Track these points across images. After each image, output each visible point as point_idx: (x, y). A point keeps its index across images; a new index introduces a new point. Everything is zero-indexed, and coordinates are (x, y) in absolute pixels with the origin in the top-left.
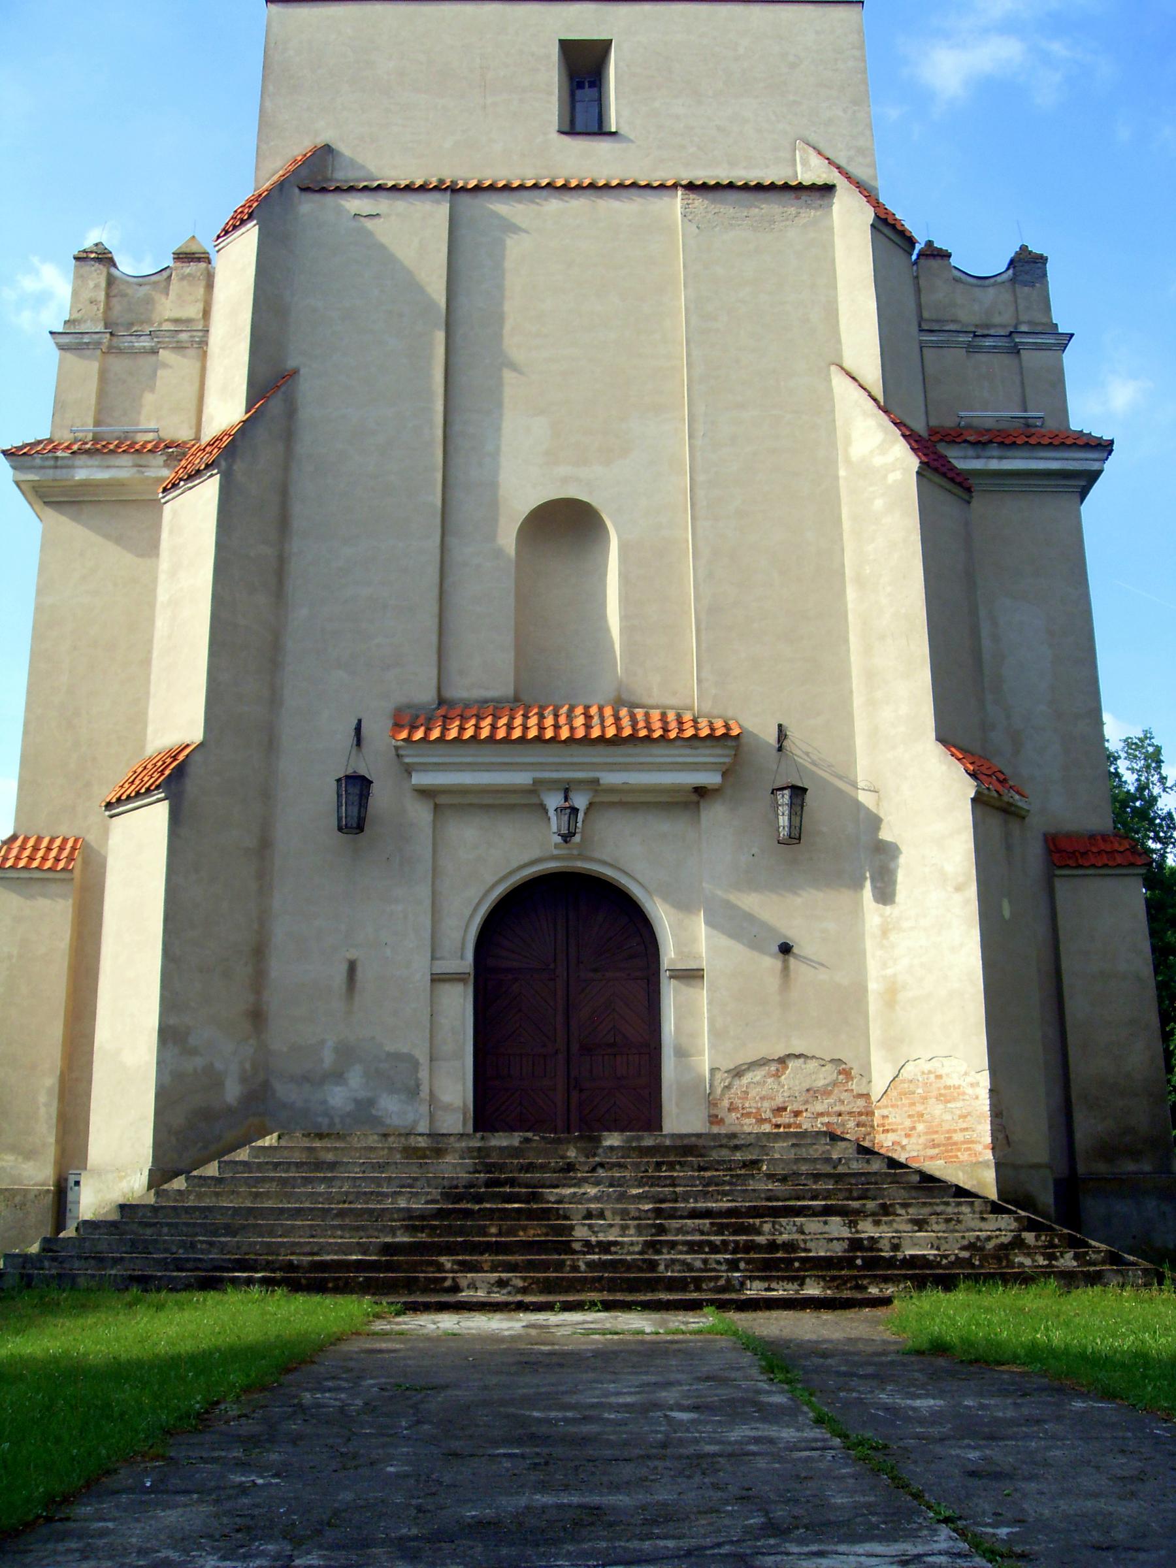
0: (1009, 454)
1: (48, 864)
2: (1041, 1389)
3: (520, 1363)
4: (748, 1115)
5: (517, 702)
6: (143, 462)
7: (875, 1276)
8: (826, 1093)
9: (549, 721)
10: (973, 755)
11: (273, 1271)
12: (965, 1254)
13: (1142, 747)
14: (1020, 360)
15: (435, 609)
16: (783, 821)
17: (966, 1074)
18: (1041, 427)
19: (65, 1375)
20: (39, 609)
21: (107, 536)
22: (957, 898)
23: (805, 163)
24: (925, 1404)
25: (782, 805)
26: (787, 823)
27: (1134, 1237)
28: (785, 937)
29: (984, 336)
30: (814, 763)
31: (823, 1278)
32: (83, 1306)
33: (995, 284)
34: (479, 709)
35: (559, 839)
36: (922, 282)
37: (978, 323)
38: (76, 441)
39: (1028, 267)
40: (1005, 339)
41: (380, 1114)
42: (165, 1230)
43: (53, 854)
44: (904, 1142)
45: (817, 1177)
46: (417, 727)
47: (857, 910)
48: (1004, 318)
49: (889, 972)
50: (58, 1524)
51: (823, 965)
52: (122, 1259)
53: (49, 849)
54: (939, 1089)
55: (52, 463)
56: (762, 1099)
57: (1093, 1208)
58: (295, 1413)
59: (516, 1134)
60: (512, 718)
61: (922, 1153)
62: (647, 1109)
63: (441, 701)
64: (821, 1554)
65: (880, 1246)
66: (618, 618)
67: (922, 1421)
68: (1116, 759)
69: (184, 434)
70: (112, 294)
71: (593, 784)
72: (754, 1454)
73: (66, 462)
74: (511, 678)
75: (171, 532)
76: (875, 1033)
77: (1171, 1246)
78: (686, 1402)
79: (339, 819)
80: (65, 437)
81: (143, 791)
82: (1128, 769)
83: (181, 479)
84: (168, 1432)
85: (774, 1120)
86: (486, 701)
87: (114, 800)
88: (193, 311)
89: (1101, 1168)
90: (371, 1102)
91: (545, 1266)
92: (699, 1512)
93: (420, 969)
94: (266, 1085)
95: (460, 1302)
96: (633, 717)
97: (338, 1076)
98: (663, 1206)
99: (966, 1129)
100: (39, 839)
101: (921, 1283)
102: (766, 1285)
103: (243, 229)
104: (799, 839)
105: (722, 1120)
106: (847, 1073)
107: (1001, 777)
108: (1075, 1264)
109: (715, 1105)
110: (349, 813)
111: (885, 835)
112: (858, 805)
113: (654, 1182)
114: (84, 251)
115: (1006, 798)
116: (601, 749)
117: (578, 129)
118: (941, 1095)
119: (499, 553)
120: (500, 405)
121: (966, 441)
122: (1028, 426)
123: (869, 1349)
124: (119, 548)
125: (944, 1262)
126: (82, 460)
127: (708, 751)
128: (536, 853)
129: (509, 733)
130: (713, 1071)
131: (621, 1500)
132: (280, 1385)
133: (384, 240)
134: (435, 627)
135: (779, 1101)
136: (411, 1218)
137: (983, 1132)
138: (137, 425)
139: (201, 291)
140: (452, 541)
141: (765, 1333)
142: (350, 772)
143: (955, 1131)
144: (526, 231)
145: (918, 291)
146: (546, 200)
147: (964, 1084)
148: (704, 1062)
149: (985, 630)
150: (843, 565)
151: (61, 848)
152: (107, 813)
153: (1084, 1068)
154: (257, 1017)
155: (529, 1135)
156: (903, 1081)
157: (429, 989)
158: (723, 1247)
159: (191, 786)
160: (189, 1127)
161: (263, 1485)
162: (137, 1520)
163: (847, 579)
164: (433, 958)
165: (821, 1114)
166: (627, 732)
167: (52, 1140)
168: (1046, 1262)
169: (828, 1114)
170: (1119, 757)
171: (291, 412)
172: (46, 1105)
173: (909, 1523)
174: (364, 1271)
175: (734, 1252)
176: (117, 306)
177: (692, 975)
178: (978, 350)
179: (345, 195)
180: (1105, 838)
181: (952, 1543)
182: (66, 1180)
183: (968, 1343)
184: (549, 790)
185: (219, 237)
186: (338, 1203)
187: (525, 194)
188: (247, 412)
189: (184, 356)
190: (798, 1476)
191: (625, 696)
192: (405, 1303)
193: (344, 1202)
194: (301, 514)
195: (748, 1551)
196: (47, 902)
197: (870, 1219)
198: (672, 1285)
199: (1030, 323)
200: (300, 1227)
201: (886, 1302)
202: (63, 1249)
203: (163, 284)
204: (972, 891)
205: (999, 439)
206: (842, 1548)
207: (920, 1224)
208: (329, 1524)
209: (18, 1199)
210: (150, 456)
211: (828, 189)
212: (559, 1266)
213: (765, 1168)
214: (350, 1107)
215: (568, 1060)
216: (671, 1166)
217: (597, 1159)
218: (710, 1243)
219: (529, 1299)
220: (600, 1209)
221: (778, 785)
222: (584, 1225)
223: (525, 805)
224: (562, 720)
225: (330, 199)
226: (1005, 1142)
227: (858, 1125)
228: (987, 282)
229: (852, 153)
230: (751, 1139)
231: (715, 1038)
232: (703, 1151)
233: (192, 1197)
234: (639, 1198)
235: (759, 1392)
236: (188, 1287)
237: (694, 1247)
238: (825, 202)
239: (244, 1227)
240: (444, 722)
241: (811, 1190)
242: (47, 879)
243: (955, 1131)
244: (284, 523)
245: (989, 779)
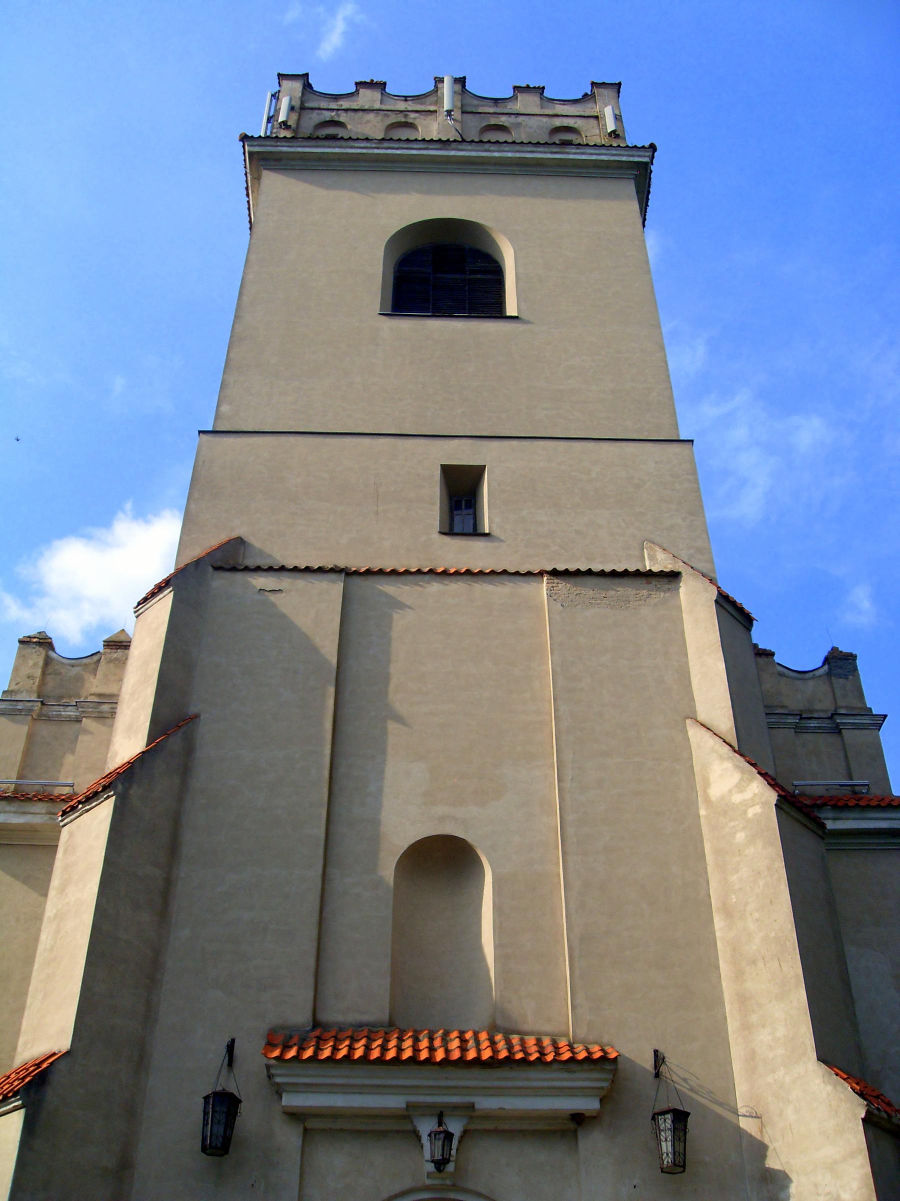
0: (843, 815)
5: (391, 1027)
9: (424, 1044)
15: (314, 934)
16: (667, 1147)
21: (15, 876)
23: (652, 558)
26: (670, 1149)
29: (810, 718)
30: (692, 1089)
33: (813, 678)
35: (431, 1167)
40: (827, 721)
46: (291, 1047)
48: (825, 705)
60: (387, 1040)
63: (316, 1024)
70: (47, 672)
74: (387, 1012)
75: (65, 852)
79: (204, 1139)
86: (361, 1025)
96: (509, 1043)
103: (161, 596)
104: (684, 1167)
111: (772, 1163)
112: (740, 1133)
114: (29, 637)
116: (476, 1072)
117: (456, 530)
120: (384, 752)
122: (854, 793)
124: (26, 887)
133: (284, 610)
134: (313, 952)
142: (219, 1089)
144: (409, 607)
146: (429, 583)
166: (503, 1054)
171: (189, 750)
176: (51, 682)
179: (252, 574)
184: (424, 1115)
187: (410, 578)
189: (104, 725)
191: (499, 1022)
199: (846, 707)
203: (93, 666)
211: (674, 576)
224: (437, 1043)
225: (239, 577)
228: (807, 676)
229: (692, 551)
238: (673, 586)
244: (174, 848)
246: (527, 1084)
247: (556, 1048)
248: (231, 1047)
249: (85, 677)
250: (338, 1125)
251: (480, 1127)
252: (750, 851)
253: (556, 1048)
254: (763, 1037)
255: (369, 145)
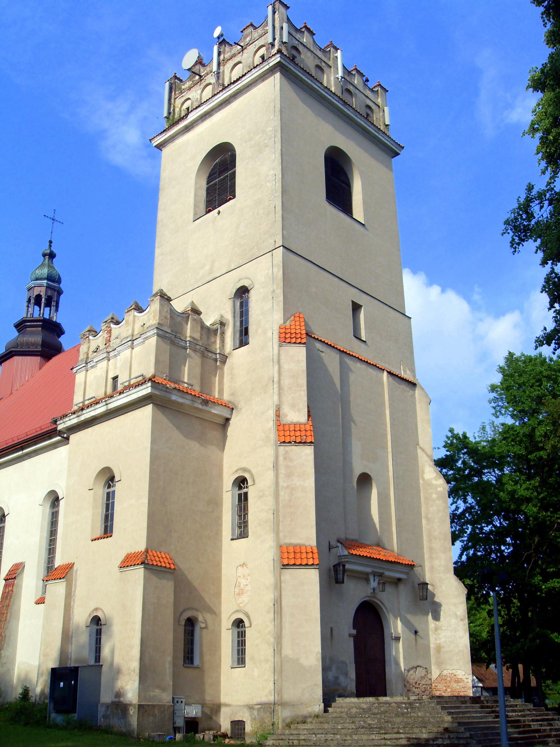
6: (194, 400)
21: (174, 425)
22: (461, 623)
49: (438, 642)
76: (433, 660)
111: (436, 599)
126: (175, 392)
130: (405, 670)
196: (166, 581)
209: (162, 708)
252: (437, 502)
254: (437, 563)
255: (320, 86)
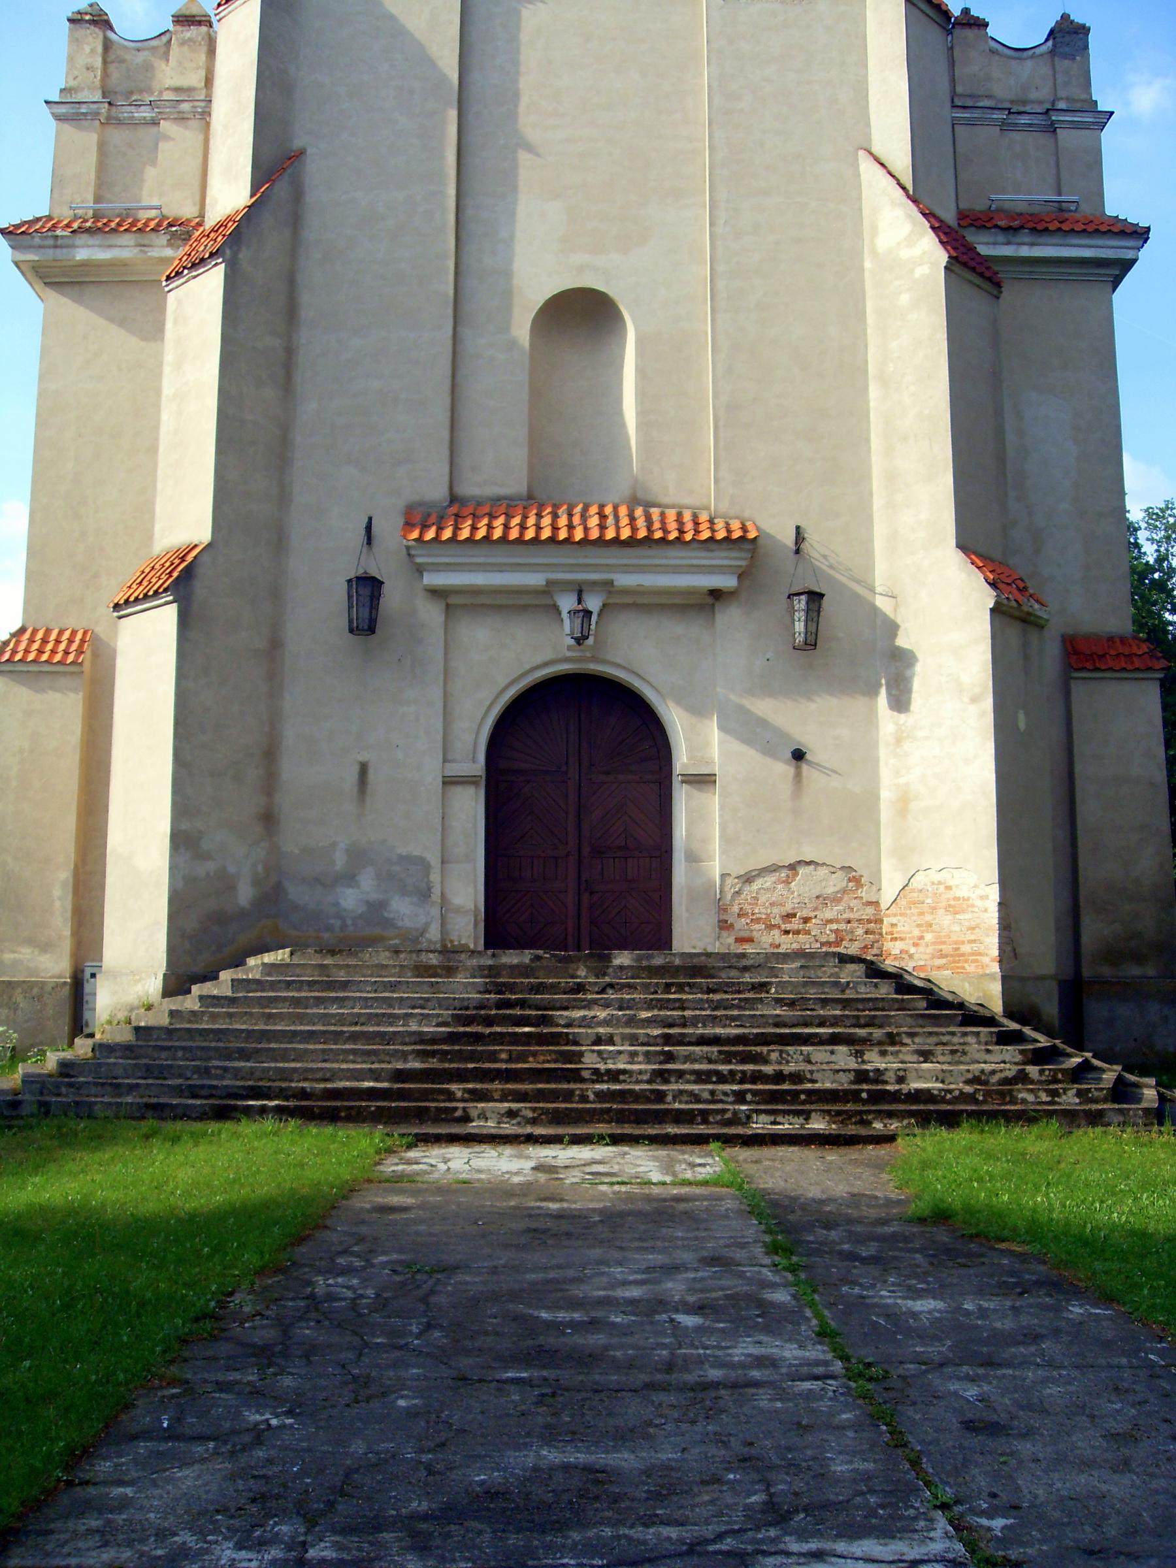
0: (1041, 240)
1: (58, 658)
2: (1039, 1284)
3: (529, 1230)
4: (758, 921)
5: (531, 501)
6: (146, 242)
7: (880, 1112)
8: (836, 900)
9: (563, 521)
10: (993, 561)
11: (287, 1099)
12: (968, 1089)
13: (1163, 517)
14: (1056, 139)
16: (799, 627)
17: (975, 886)
18: (1076, 211)
19: (84, 1235)
20: (42, 395)
21: (111, 319)
22: (973, 709)
24: (925, 1306)
25: (798, 611)
26: (803, 630)
27: (1135, 1040)
28: (799, 743)
29: (1019, 113)
30: (831, 567)
31: (829, 1112)
32: (100, 1137)
33: (1032, 57)
34: (492, 507)
35: (572, 642)
36: (957, 53)
37: (1013, 98)
38: (76, 217)
39: (1069, 37)
41: (392, 916)
42: (180, 1054)
43: (62, 646)
44: (912, 950)
45: (825, 1002)
47: (871, 719)
48: (1041, 93)
49: (902, 781)
50: (78, 1489)
51: (835, 772)
52: (138, 1085)
53: (58, 641)
54: (948, 900)
55: (51, 242)
56: (772, 904)
57: (1096, 1010)
58: (307, 1309)
59: (527, 951)
61: (929, 963)
62: (658, 934)
63: (454, 499)
64: (819, 1556)
65: (885, 1078)
66: (634, 415)
67: (922, 1336)
68: (1136, 530)
69: (188, 211)
70: (109, 60)
71: (607, 586)
72: (756, 1384)
73: (66, 241)
74: (524, 474)
75: (175, 322)
76: (886, 842)
77: (1171, 1049)
78: (691, 1299)
79: (350, 621)
80: (65, 214)
81: (151, 593)
82: (1148, 539)
83: (185, 268)
84: (184, 1341)
85: (783, 927)
87: (122, 602)
88: (195, 79)
89: (1106, 971)
90: (382, 905)
91: (553, 1096)
92: (703, 1482)
93: (431, 772)
94: (278, 888)
95: (470, 1134)
97: (349, 878)
98: (671, 1031)
99: (973, 941)
100: (48, 632)
101: (924, 1120)
102: (772, 1118)
105: (732, 925)
106: (857, 881)
107: (1021, 585)
108: (1077, 1101)
109: (725, 910)
110: (360, 615)
111: (902, 642)
112: (875, 610)
113: (664, 1005)
114: (79, 13)
115: (1025, 608)
116: (615, 551)
118: (950, 906)
119: (513, 344)
120: (514, 189)
121: (996, 226)
122: (1061, 210)
123: (873, 1213)
124: (123, 331)
125: (949, 1096)
127: (724, 554)
128: (549, 655)
129: (522, 534)
131: (625, 1459)
132: (294, 1264)
134: (447, 422)
135: (788, 908)
136: (422, 1042)
137: (991, 944)
138: (139, 202)
139: (203, 57)
140: (466, 332)
141: (770, 1185)
142: (360, 572)
143: (963, 943)
145: (952, 63)
147: (973, 896)
148: (715, 868)
149: (1011, 438)
150: (867, 361)
151: (71, 641)
152: (116, 614)
153: (1093, 872)
154: (269, 819)
155: (540, 952)
156: (913, 891)
157: (440, 791)
158: (730, 1078)
159: (199, 588)
160: (202, 942)
161: (278, 1427)
162: (155, 1484)
163: (870, 377)
164: (445, 761)
165: (831, 921)
166: (642, 533)
167: (67, 933)
168: (1049, 1099)
169: (837, 921)
170: (1140, 528)
171: (298, 195)
172: (60, 898)
173: (907, 1508)
174: (376, 1100)
175: (741, 1082)
176: (115, 72)
177: (704, 780)
178: (1014, 127)
180: (1123, 640)
181: (948, 1544)
182: (83, 971)
183: (969, 1210)
185: (219, 5)
186: (351, 1025)
188: (252, 196)
189: (187, 128)
190: (799, 1424)
191: (640, 495)
192: (416, 1135)
193: (356, 1024)
194: (309, 304)
195: (750, 1548)
196: (58, 696)
197: (876, 1049)
198: (680, 1117)
199: (1067, 99)
200: (313, 1051)
201: (890, 1139)
202: (81, 1074)
203: (163, 49)
204: (988, 703)
205: (1031, 225)
206: (841, 1546)
207: (926, 1056)
208: (343, 1493)
209: (35, 991)
210: (153, 235)
212: (568, 1096)
213: (773, 990)
214: (362, 909)
215: (580, 862)
216: (681, 988)
217: (608, 979)
218: (717, 1073)
219: (539, 1131)
220: (611, 1035)
221: (795, 589)
222: (593, 1051)
223: (537, 606)
224: (576, 520)
226: (1012, 955)
227: (866, 933)
228: (1025, 54)
230: (761, 959)
231: (728, 839)
232: (712, 971)
233: (206, 1018)
234: (649, 1022)
235: (765, 1284)
236: (202, 1116)
237: (701, 1077)
239: (258, 1051)
240: (456, 521)
241: (819, 1015)
242: (58, 673)
243: (963, 943)
244: (291, 312)
245: (1009, 589)
246: (664, 562)
247: (696, 523)
248: (369, 528)
249: (155, 65)
250: (479, 600)
251: (618, 601)
253: (696, 523)
